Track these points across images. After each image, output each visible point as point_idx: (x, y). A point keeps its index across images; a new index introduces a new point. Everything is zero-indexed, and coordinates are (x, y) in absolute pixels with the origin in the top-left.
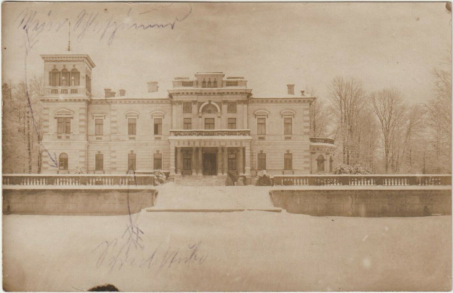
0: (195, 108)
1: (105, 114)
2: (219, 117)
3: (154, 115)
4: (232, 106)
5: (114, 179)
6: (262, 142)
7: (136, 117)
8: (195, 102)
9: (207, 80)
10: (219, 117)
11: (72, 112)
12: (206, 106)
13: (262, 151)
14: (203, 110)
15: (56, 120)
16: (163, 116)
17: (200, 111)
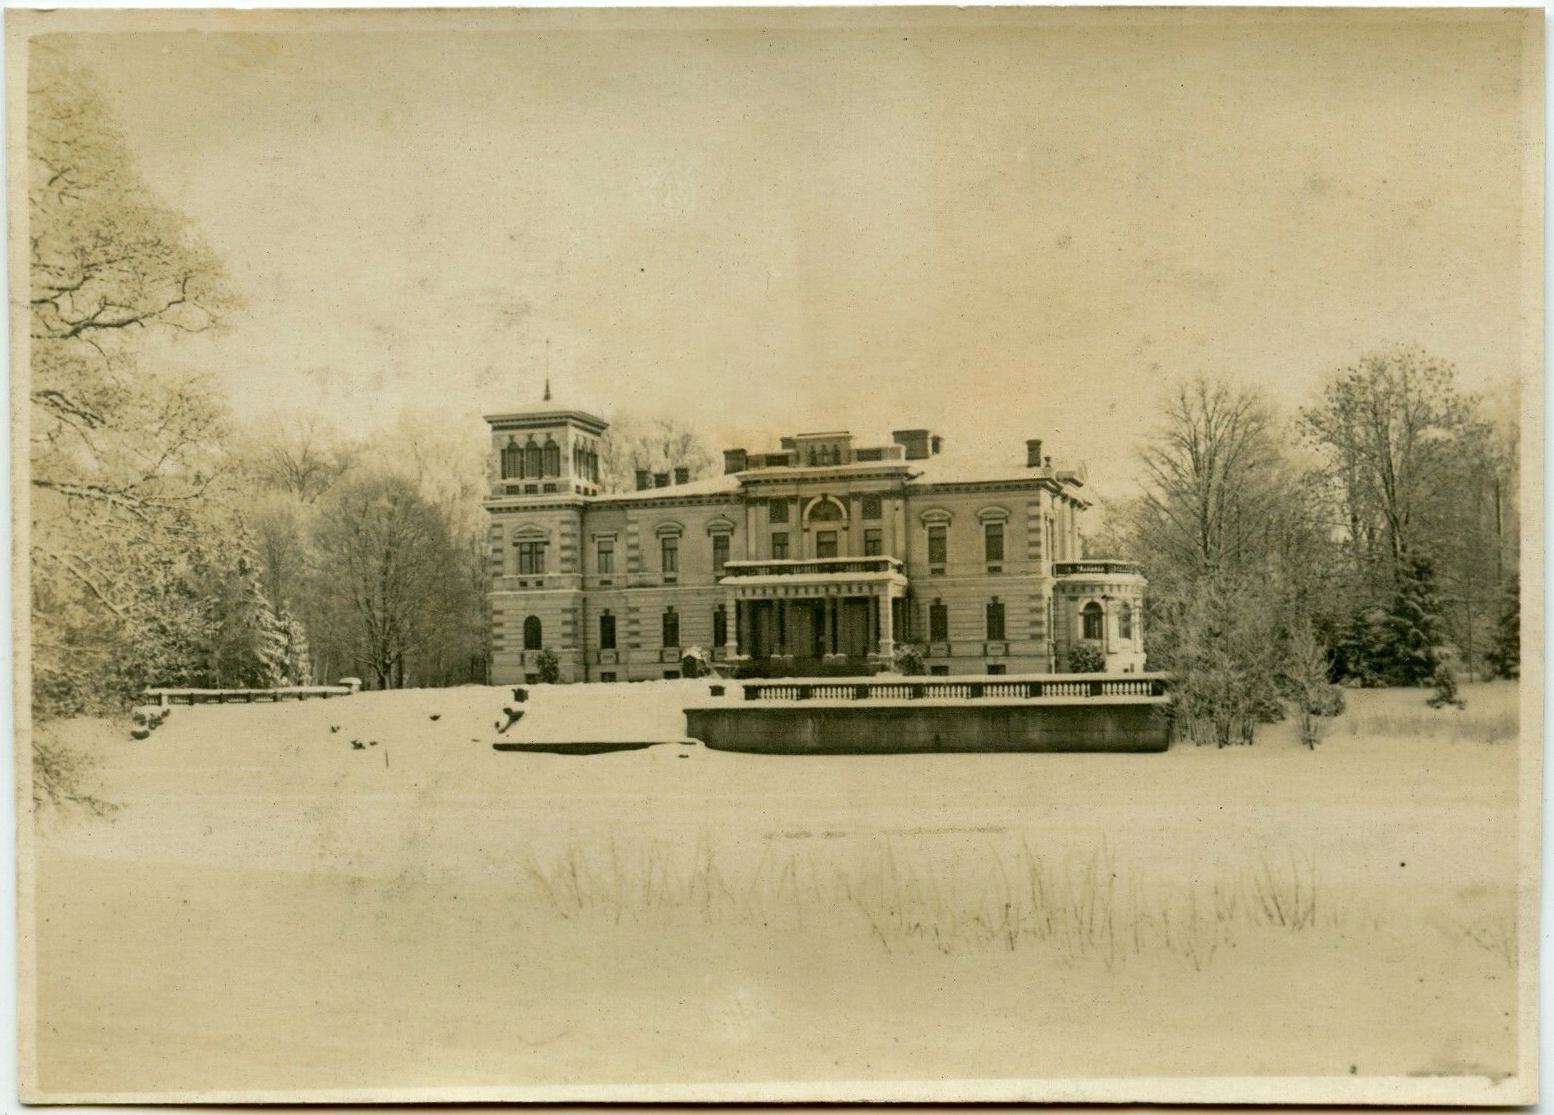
2: (846, 529)
3: (714, 528)
6: (940, 580)
7: (613, 539)
8: (793, 499)
9: (818, 449)
12: (817, 506)
13: (938, 600)
14: (813, 515)
15: (516, 549)
16: (732, 530)
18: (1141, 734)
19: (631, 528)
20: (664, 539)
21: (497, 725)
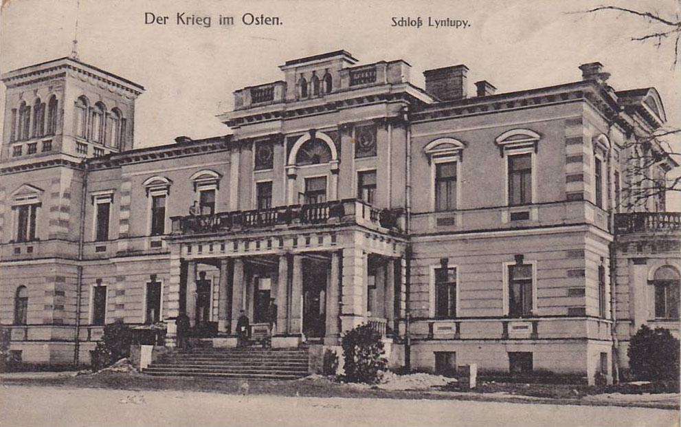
1: (111, 192)
2: (336, 172)
8: (277, 139)
10: (336, 172)
12: (305, 146)
14: (301, 157)
19: (127, 186)
21: (168, 18)
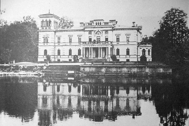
0: (93, 32)
4: (106, 31)
5: (15, 61)
7: (60, 37)
8: (93, 31)
11: (49, 36)
17: (95, 34)
18: (92, 110)
20: (79, 37)
